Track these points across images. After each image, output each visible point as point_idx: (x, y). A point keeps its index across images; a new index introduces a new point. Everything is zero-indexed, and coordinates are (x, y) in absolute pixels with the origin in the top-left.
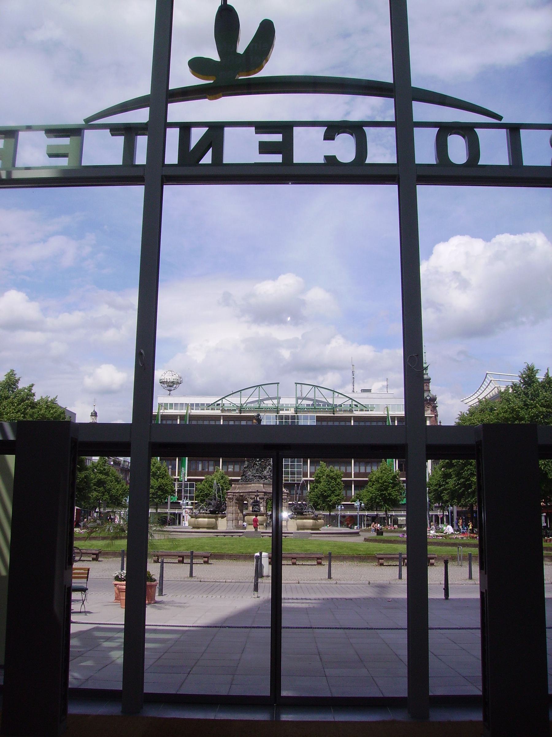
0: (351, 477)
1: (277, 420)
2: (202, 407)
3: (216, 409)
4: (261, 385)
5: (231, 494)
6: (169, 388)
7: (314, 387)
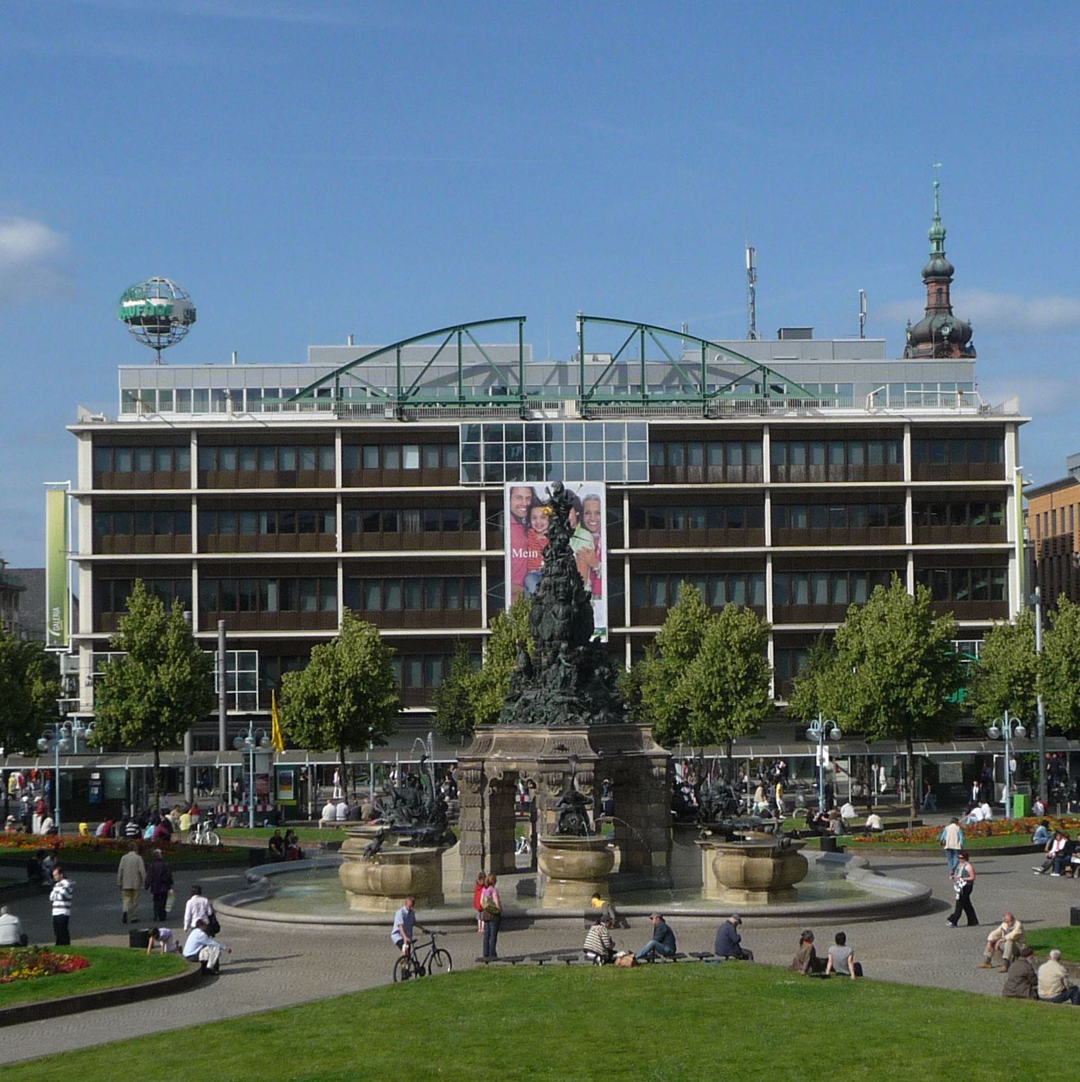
0: (622, 547)
1: (751, 567)
2: (272, 401)
3: (280, 406)
4: (464, 326)
5: (474, 764)
6: (154, 338)
7: (639, 331)
